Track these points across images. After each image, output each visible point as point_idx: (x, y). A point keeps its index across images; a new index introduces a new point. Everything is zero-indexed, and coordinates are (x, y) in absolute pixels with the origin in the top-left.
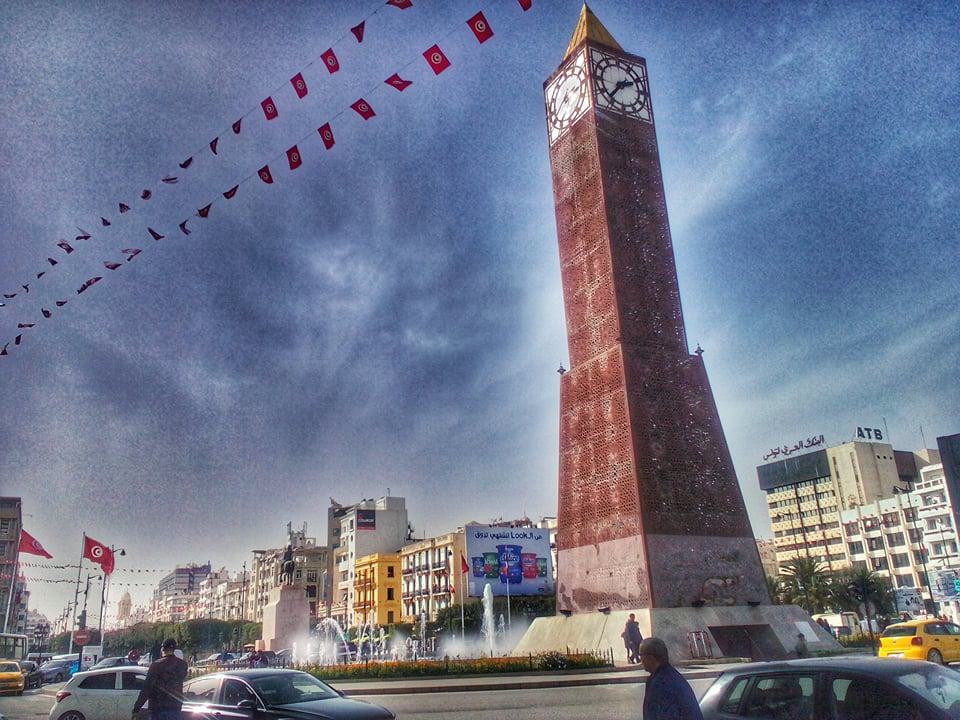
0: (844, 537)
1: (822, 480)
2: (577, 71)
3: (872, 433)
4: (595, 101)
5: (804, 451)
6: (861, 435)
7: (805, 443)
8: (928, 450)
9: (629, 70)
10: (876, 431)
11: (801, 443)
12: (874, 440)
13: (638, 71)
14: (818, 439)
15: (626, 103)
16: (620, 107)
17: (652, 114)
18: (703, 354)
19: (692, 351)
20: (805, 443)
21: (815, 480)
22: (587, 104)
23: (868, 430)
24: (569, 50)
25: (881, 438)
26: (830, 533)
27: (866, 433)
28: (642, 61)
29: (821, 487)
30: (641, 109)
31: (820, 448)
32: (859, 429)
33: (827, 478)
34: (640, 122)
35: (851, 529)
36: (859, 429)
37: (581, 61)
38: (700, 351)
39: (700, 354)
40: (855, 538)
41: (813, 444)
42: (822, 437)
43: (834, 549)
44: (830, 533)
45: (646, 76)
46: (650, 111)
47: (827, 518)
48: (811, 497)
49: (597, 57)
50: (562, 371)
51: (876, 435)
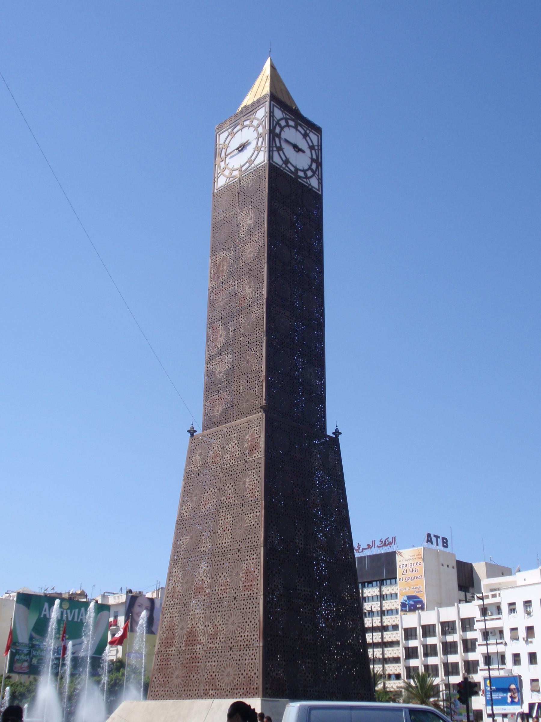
0: (402, 641)
1: (388, 581)
2: (255, 123)
3: (440, 540)
4: (270, 157)
5: (375, 551)
6: (429, 540)
7: (378, 543)
8: (486, 563)
9: (305, 136)
10: (443, 538)
11: (374, 542)
12: (440, 547)
13: (314, 137)
14: (390, 540)
15: (300, 167)
16: (293, 169)
17: (322, 183)
18: (340, 437)
19: (330, 432)
20: (378, 543)
21: (382, 582)
22: (262, 158)
23: (437, 537)
24: (248, 100)
25: (447, 547)
26: (389, 636)
27: (434, 539)
28: (318, 130)
29: (387, 590)
30: (311, 177)
31: (391, 550)
32: (429, 535)
33: (393, 581)
34: (309, 190)
35: (410, 633)
36: (429, 535)
37: (262, 113)
38: (337, 433)
39: (337, 437)
40: (412, 643)
41: (385, 545)
42: (394, 539)
43: (390, 652)
44: (389, 636)
45: (320, 146)
46: (320, 181)
47: (388, 621)
48: (375, 598)
49: (278, 114)
50: (192, 432)
51: (443, 542)
